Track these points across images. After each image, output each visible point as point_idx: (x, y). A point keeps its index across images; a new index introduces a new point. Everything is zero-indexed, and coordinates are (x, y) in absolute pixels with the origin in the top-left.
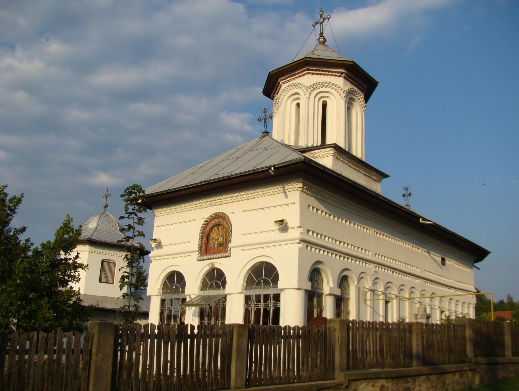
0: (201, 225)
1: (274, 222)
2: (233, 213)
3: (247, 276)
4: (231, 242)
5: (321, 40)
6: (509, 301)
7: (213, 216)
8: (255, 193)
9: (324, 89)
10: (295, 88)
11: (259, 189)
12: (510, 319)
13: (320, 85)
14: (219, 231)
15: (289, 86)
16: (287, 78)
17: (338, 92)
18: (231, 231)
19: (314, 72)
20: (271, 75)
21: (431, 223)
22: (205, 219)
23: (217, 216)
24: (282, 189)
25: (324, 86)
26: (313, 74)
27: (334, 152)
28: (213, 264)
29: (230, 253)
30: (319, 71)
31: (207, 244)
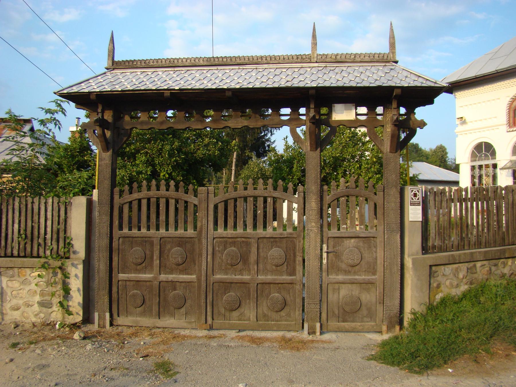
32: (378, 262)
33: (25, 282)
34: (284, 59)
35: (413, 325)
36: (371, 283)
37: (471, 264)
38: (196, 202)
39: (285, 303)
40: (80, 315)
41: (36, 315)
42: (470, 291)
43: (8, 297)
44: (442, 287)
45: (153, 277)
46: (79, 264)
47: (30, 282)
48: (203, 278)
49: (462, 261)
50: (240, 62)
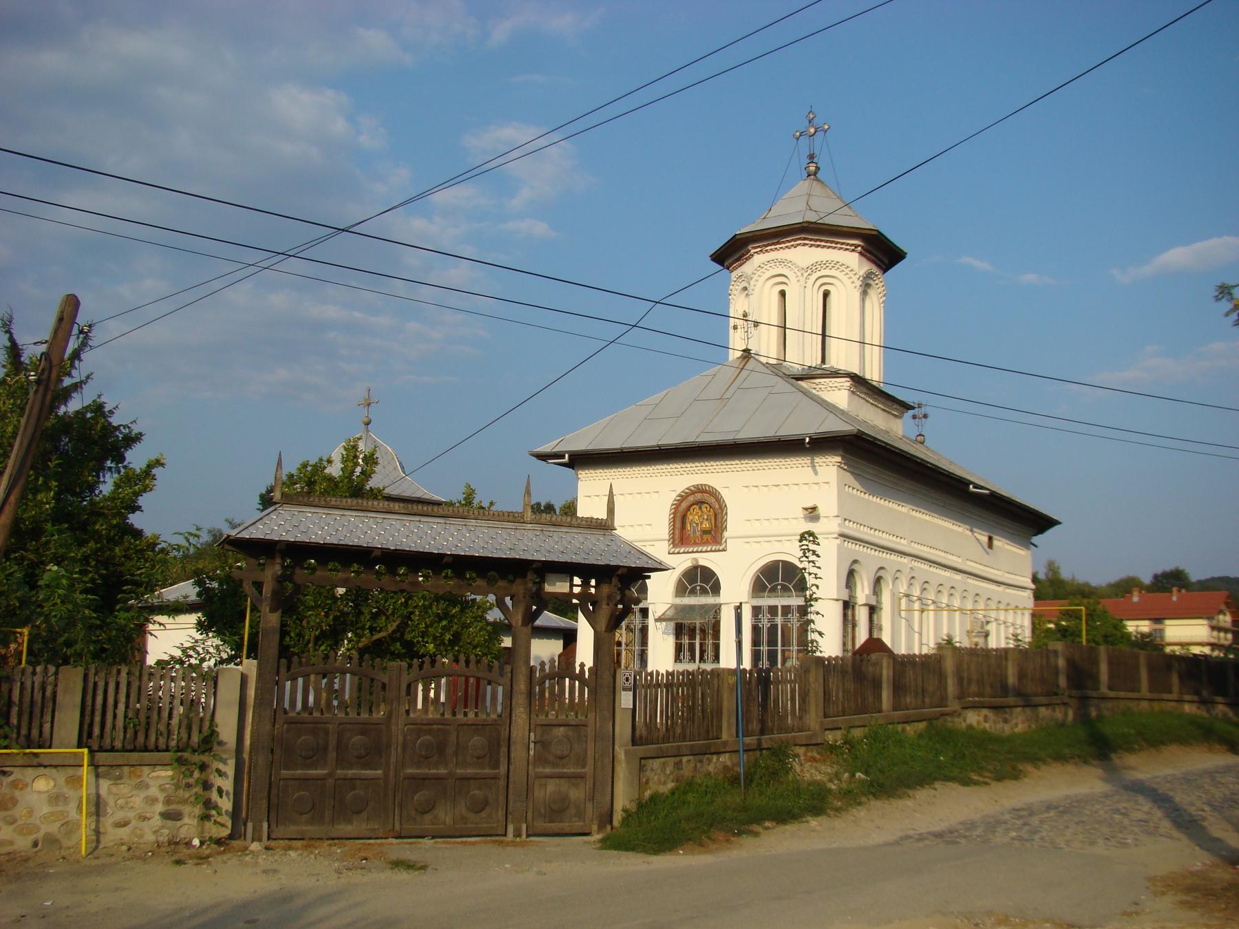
1: (801, 510)
3: (754, 578)
6: (1050, 574)
7: (693, 489)
9: (827, 272)
11: (773, 458)
12: (1055, 619)
18: (726, 514)
19: (812, 243)
20: (738, 239)
21: (987, 492)
22: (678, 492)
24: (810, 461)
25: (827, 267)
26: (812, 246)
27: (851, 384)
28: (696, 560)
29: (726, 546)
30: (821, 241)
32: (589, 753)
33: (143, 786)
34: (494, 514)
35: (625, 821)
36: (581, 777)
37: (678, 759)
38: (386, 680)
39: (486, 803)
40: (227, 827)
41: (155, 832)
42: (677, 788)
43: (108, 808)
44: (651, 784)
45: (327, 773)
46: (231, 758)
47: (147, 785)
48: (392, 773)
49: (669, 755)
50: (443, 513)
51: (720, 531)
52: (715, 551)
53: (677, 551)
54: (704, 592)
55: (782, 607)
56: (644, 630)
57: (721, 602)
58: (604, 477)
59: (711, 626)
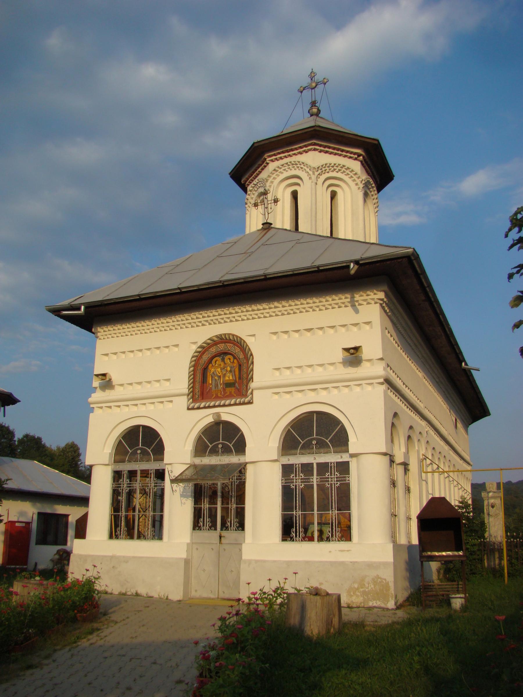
0: (191, 354)
2: (254, 335)
4: (253, 381)
5: (315, 110)
7: (215, 339)
8: (216, 316)
9: (339, 175)
10: (293, 169)
13: (330, 168)
14: (225, 364)
15: (283, 165)
16: (279, 153)
17: (354, 180)
18: (253, 363)
19: (322, 148)
22: (199, 344)
23: (222, 339)
24: (349, 300)
25: (335, 170)
28: (218, 415)
29: (252, 398)
30: (329, 148)
31: (203, 383)
51: (245, 381)
52: (240, 404)
53: (197, 405)
54: (227, 451)
55: (318, 464)
56: (160, 496)
57: (247, 461)
58: (123, 334)
59: (234, 487)
